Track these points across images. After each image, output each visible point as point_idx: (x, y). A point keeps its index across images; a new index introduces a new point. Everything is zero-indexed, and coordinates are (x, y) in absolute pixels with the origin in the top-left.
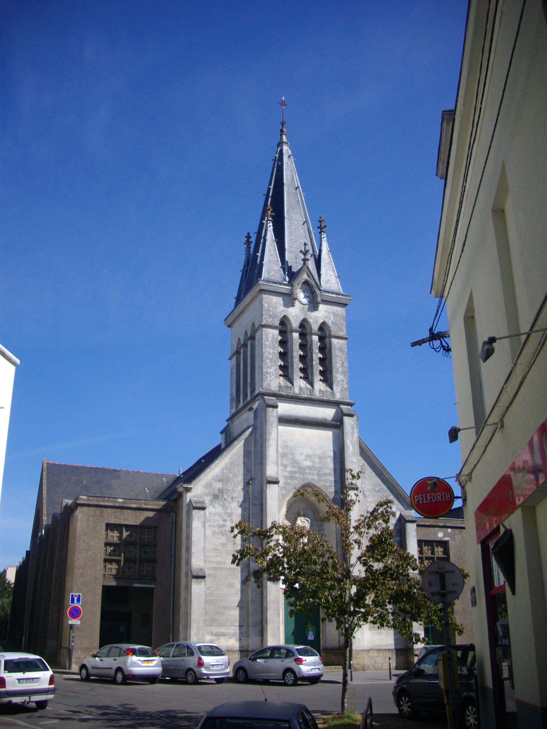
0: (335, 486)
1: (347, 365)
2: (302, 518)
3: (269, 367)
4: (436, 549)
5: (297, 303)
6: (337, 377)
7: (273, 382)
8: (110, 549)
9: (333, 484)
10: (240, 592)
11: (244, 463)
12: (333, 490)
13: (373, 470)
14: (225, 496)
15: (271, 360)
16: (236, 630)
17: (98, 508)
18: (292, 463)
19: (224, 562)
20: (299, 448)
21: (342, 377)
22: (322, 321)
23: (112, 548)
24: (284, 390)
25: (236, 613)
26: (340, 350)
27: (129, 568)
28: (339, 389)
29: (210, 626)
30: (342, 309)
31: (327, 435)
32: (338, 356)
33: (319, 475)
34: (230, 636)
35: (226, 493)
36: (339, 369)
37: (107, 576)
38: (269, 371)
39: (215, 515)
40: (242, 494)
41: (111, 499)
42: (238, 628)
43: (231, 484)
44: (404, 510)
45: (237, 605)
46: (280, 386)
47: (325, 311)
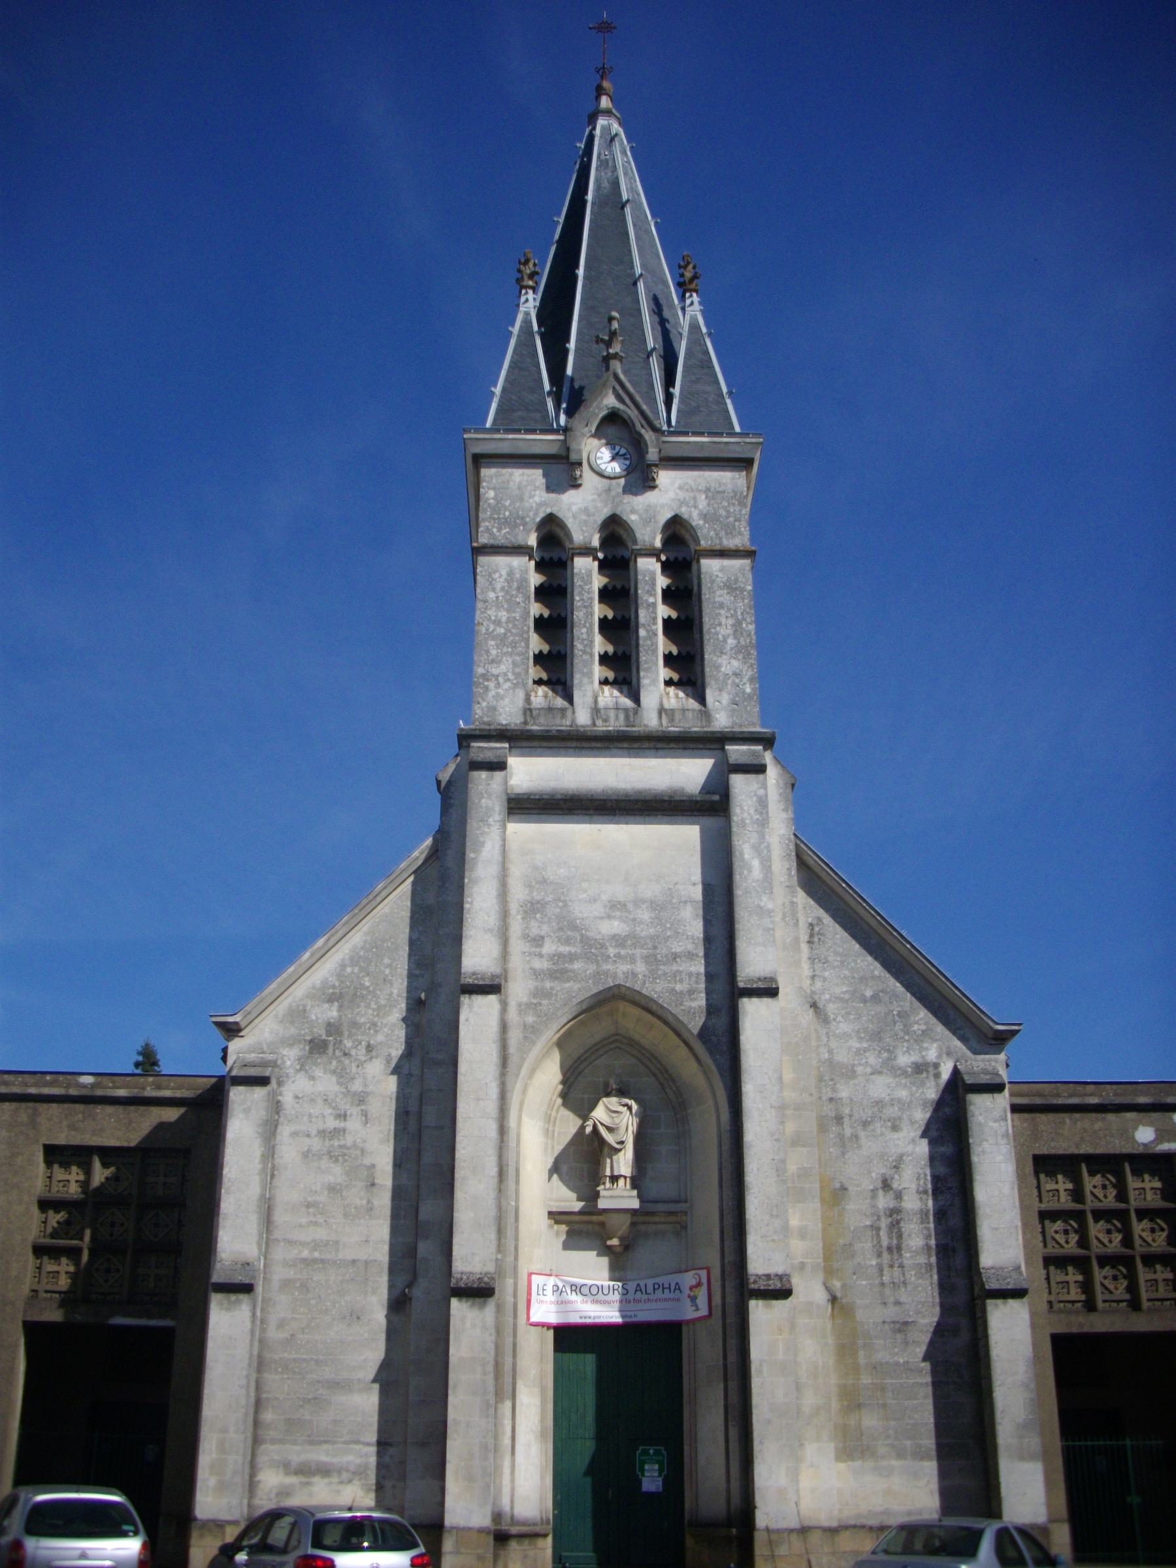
0: (708, 992)
1: (752, 627)
2: (613, 1102)
3: (493, 661)
4: (1132, 1183)
5: (588, 478)
6: (718, 667)
7: (507, 701)
8: (55, 1218)
9: (702, 986)
10: (383, 1336)
11: (412, 943)
12: (703, 1002)
13: (854, 936)
14: (348, 1044)
15: (502, 639)
16: (368, 1455)
17: (23, 1105)
18: (561, 929)
19: (337, 1243)
20: (585, 885)
21: (735, 663)
22: (669, 515)
23: (62, 1216)
24: (542, 720)
25: (368, 1402)
26: (731, 587)
27: (108, 1271)
28: (725, 698)
29: (282, 1441)
30: (736, 474)
31: (685, 837)
32: (722, 606)
33: (651, 960)
34: (345, 1476)
35: (350, 1036)
36: (725, 641)
37: (43, 1295)
38: (495, 671)
39: (312, 1100)
40: (401, 1033)
41: (61, 1078)
42: (374, 1449)
43: (368, 1006)
44: (969, 1053)
45: (371, 1376)
46: (528, 711)
47: (680, 488)
